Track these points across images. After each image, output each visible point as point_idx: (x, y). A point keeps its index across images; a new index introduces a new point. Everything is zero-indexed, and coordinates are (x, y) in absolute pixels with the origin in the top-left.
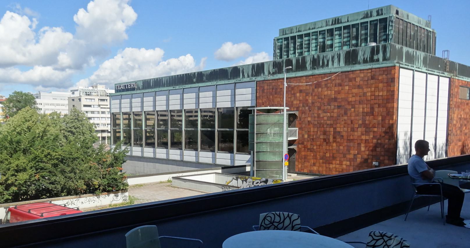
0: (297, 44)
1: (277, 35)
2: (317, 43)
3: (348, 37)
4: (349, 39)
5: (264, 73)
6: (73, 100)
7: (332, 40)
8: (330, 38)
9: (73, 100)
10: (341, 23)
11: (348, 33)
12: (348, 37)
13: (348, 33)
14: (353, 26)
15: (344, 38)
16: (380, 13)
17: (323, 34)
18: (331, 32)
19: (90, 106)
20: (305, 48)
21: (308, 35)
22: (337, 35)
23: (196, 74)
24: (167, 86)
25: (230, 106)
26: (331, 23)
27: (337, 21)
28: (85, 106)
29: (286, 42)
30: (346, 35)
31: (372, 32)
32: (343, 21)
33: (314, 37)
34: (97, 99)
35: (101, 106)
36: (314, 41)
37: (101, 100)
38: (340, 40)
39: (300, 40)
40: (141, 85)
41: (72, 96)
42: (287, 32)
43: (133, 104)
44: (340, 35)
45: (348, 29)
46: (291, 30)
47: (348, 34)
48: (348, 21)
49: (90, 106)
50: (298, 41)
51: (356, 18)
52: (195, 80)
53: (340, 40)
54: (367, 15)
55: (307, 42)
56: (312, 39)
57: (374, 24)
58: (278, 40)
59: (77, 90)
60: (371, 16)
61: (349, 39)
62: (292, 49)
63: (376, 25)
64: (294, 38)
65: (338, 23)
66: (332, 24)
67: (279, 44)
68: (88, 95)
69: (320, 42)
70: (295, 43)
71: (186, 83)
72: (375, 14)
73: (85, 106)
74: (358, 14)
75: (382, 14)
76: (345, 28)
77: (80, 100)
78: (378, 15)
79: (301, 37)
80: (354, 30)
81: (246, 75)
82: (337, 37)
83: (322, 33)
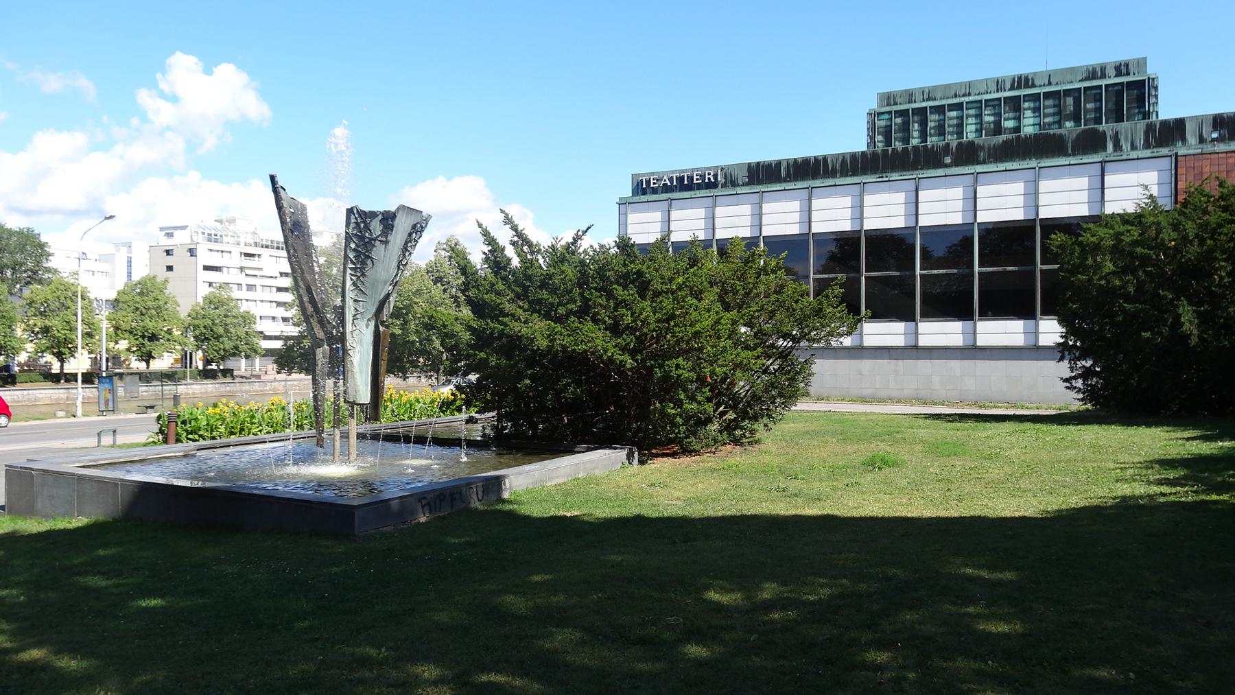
0: (931, 124)
1: (873, 105)
2: (981, 123)
3: (1054, 114)
4: (1057, 118)
5: (1184, 140)
6: (168, 252)
7: (1018, 119)
8: (1011, 115)
9: (168, 252)
10: (1033, 86)
11: (1055, 106)
12: (1054, 114)
13: (1055, 106)
14: (1067, 93)
15: (1046, 116)
16: (1124, 71)
17: (994, 107)
18: (1015, 105)
19: (217, 269)
20: (951, 134)
21: (959, 107)
22: (1029, 109)
23: (784, 165)
24: (842, 176)
25: (849, 229)
26: (1008, 86)
27: (1022, 82)
28: (206, 268)
29: (899, 120)
30: (1051, 110)
31: (1111, 106)
32: (1037, 83)
33: (972, 112)
34: (236, 251)
35: (248, 272)
36: (972, 120)
37: (247, 255)
38: (1037, 121)
39: (935, 117)
40: (742, 176)
41: (166, 242)
42: (899, 101)
43: (717, 221)
44: (1036, 110)
45: (1034, 101)
46: (910, 96)
47: (1056, 110)
48: (1050, 83)
49: (217, 269)
50: (933, 119)
51: (1069, 78)
52: (948, 160)
53: (1037, 121)
54: (1092, 74)
55: (955, 122)
56: (968, 116)
57: (1116, 92)
58: (879, 114)
59: (185, 227)
60: (1103, 76)
61: (1057, 118)
62: (916, 134)
63: (1119, 94)
64: (922, 112)
65: (1027, 86)
66: (1012, 88)
67: (883, 123)
68: (216, 241)
69: (989, 123)
70: (924, 123)
71: (814, 177)
72: (1111, 72)
73: (206, 268)
74: (1072, 70)
75: (1128, 74)
76: (1047, 95)
77: (192, 252)
78: (1119, 74)
79: (940, 110)
80: (1070, 101)
81: (1126, 146)
82: (1029, 113)
83: (994, 104)
